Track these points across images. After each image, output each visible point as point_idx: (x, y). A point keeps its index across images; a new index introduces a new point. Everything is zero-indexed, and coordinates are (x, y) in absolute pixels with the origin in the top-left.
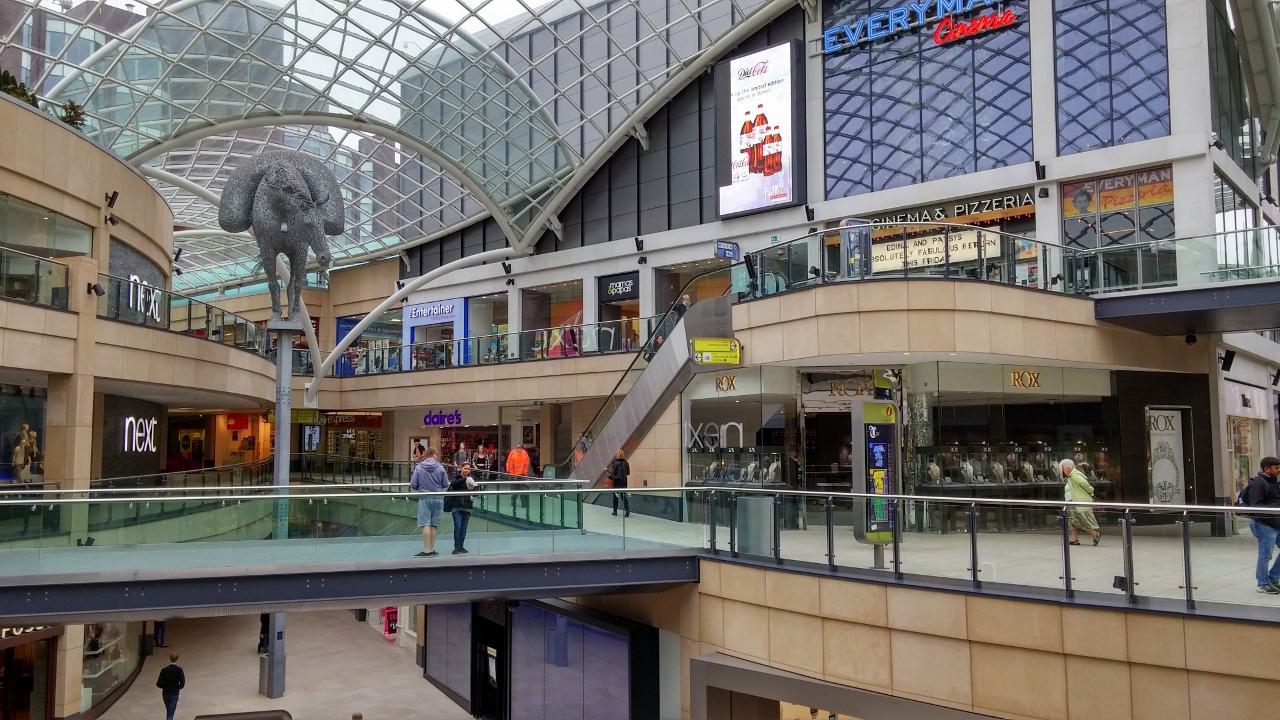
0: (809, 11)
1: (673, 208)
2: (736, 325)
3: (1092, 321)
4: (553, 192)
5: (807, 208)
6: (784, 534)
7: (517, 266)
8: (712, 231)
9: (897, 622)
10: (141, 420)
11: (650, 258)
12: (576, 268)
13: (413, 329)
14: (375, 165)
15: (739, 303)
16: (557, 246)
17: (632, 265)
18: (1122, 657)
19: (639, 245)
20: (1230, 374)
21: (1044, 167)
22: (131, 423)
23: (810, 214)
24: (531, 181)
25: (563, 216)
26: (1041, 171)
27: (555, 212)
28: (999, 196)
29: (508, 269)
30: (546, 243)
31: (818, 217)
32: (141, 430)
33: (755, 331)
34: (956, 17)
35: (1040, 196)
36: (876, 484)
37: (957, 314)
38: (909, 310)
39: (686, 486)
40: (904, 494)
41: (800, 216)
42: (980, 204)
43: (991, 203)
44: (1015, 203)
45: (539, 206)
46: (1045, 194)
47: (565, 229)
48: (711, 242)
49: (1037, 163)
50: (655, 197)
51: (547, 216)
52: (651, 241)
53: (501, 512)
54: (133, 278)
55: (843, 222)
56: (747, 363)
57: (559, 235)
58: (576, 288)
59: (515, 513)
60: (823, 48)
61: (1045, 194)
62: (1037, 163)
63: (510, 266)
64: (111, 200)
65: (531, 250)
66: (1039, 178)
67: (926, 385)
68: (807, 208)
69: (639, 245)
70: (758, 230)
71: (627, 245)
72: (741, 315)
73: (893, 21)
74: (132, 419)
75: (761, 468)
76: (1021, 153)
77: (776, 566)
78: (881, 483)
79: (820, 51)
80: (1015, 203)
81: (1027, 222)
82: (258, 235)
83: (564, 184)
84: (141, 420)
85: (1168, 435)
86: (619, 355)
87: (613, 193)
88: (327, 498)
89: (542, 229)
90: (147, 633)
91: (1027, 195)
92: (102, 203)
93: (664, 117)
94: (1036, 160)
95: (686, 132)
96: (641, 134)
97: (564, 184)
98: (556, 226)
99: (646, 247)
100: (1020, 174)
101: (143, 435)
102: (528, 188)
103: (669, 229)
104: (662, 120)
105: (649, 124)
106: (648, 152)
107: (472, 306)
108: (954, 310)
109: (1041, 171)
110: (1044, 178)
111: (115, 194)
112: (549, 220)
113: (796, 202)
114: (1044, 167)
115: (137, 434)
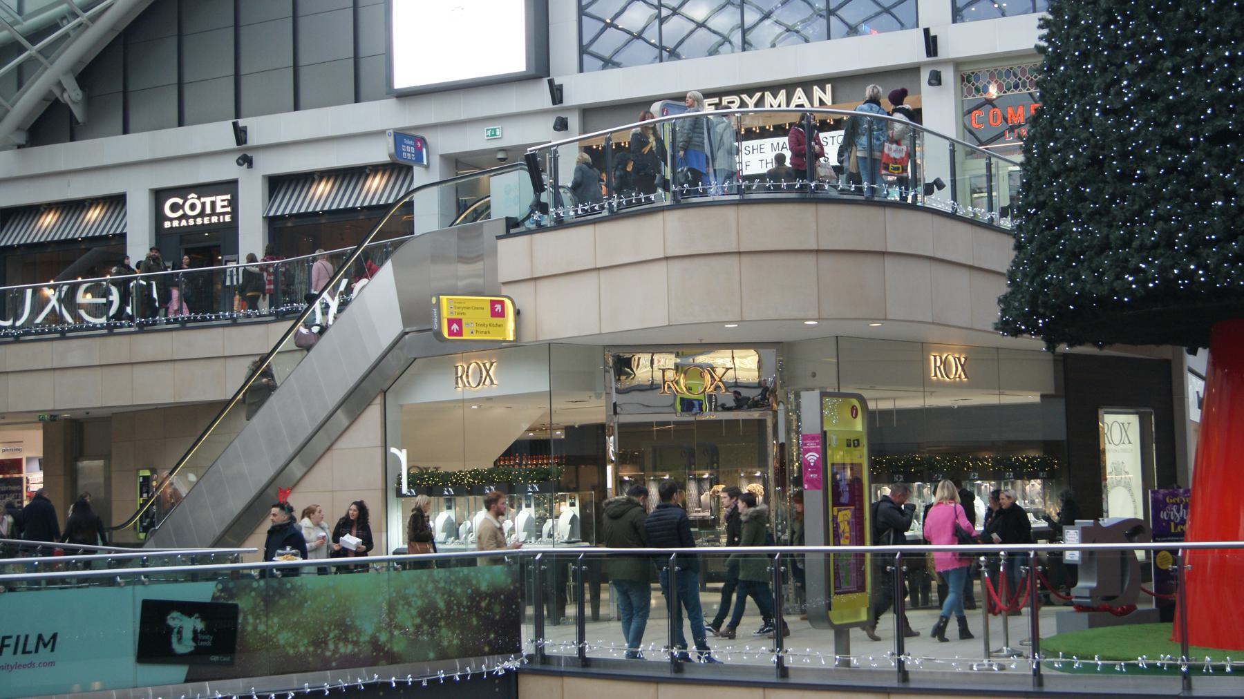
1: (303, 73)
2: (505, 274)
4: (66, 36)
5: (551, 82)
6: (548, 630)
7: (261, 129)
8: (379, 115)
11: (258, 159)
12: (112, 173)
15: (508, 235)
16: (73, 132)
17: (227, 170)
19: (240, 135)
21: (935, 37)
23: (557, 93)
24: (20, 11)
26: (931, 44)
27: (71, 70)
33: (543, 285)
35: (930, 84)
37: (888, 260)
38: (817, 251)
39: (394, 553)
40: (875, 543)
41: (540, 97)
45: (42, 59)
46: (936, 79)
48: (381, 133)
49: (927, 31)
50: (268, 49)
52: (261, 129)
55: (656, 107)
56: (528, 337)
57: (78, 112)
61: (936, 79)
62: (927, 31)
65: (21, 138)
66: (929, 54)
67: (814, 375)
68: (551, 82)
69: (240, 135)
70: (463, 117)
71: (220, 134)
72: (513, 256)
75: (543, 520)
76: (886, 16)
77: (580, 670)
78: (847, 529)
83: (93, 19)
85: (1124, 451)
86: (221, 330)
87: (244, 32)
88: (901, 550)
89: (45, 99)
94: (923, 25)
97: (93, 19)
98: (73, 95)
99: (253, 139)
100: (900, 48)
102: (17, 23)
103: (296, 108)
108: (883, 253)
109: (931, 44)
112: (59, 84)
113: (533, 72)
114: (935, 37)
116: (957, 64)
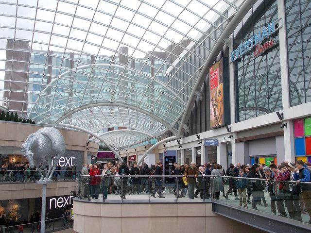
3: (212, 214)
23: (229, 130)
26: (281, 116)
30: (186, 135)
31: (232, 131)
41: (224, 131)
63: (282, 114)
71: (195, 136)
73: (245, 47)
92: (85, 145)
98: (186, 127)
99: (167, 146)
100: (271, 118)
109: (281, 116)
116: (290, 120)
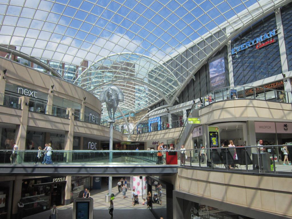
0: (228, 46)
9: (211, 180)
10: (92, 143)
13: (151, 124)
14: (82, 68)
18: (205, 179)
20: (227, 33)
22: (90, 143)
25: (179, 98)
26: (284, 76)
28: (275, 83)
29: (168, 110)
30: (176, 103)
32: (92, 144)
34: (261, 42)
36: (213, 142)
42: (270, 85)
43: (273, 85)
44: (279, 84)
47: (179, 100)
51: (175, 98)
53: (192, 165)
54: (90, 114)
57: (178, 101)
58: (182, 112)
59: (191, 165)
60: (231, 53)
61: (286, 81)
63: (285, 75)
64: (85, 99)
74: (90, 142)
79: (231, 54)
80: (279, 84)
81: (282, 88)
82: (106, 102)
84: (92, 143)
90: (91, 186)
91: (282, 82)
93: (198, 73)
95: (203, 75)
96: (194, 77)
98: (177, 99)
100: (279, 77)
101: (93, 146)
104: (198, 74)
105: (196, 75)
106: (195, 81)
107: (162, 118)
109: (284, 76)
110: (285, 77)
111: (85, 98)
115: (91, 146)
